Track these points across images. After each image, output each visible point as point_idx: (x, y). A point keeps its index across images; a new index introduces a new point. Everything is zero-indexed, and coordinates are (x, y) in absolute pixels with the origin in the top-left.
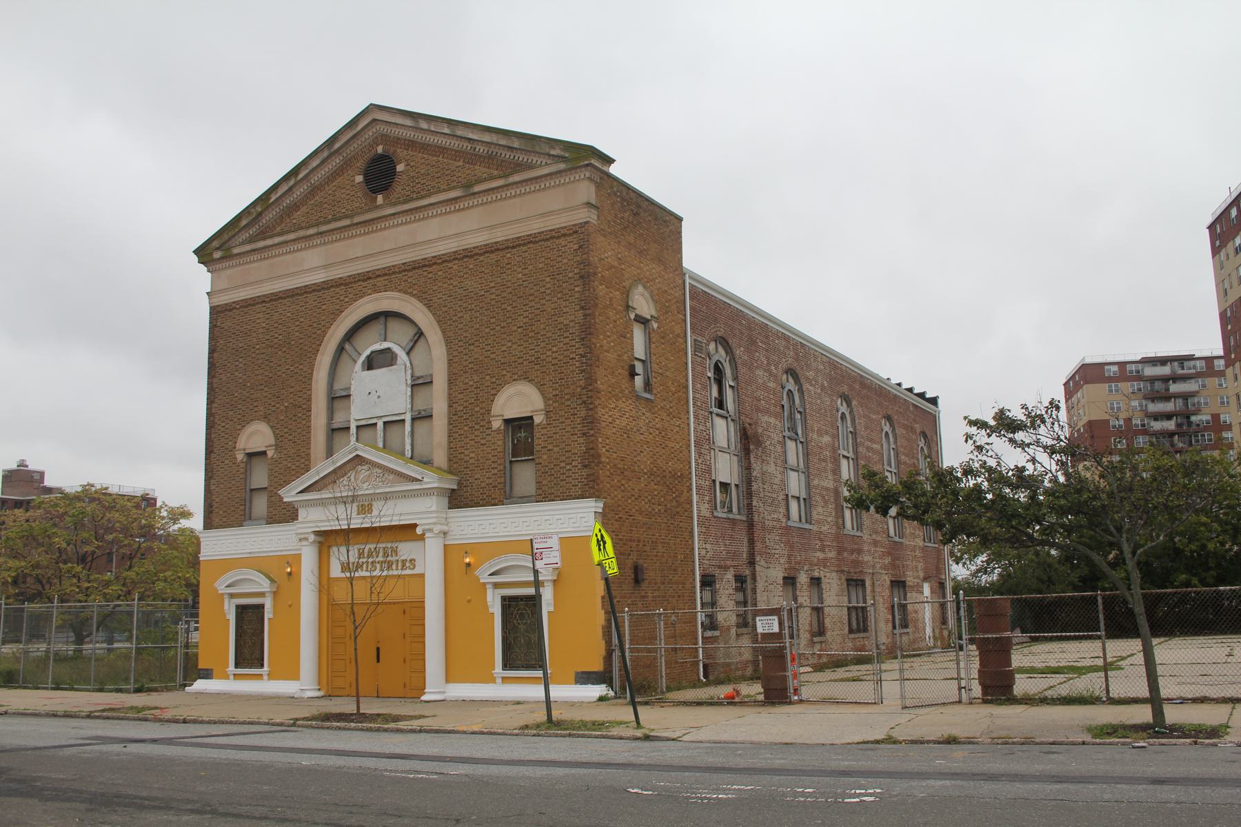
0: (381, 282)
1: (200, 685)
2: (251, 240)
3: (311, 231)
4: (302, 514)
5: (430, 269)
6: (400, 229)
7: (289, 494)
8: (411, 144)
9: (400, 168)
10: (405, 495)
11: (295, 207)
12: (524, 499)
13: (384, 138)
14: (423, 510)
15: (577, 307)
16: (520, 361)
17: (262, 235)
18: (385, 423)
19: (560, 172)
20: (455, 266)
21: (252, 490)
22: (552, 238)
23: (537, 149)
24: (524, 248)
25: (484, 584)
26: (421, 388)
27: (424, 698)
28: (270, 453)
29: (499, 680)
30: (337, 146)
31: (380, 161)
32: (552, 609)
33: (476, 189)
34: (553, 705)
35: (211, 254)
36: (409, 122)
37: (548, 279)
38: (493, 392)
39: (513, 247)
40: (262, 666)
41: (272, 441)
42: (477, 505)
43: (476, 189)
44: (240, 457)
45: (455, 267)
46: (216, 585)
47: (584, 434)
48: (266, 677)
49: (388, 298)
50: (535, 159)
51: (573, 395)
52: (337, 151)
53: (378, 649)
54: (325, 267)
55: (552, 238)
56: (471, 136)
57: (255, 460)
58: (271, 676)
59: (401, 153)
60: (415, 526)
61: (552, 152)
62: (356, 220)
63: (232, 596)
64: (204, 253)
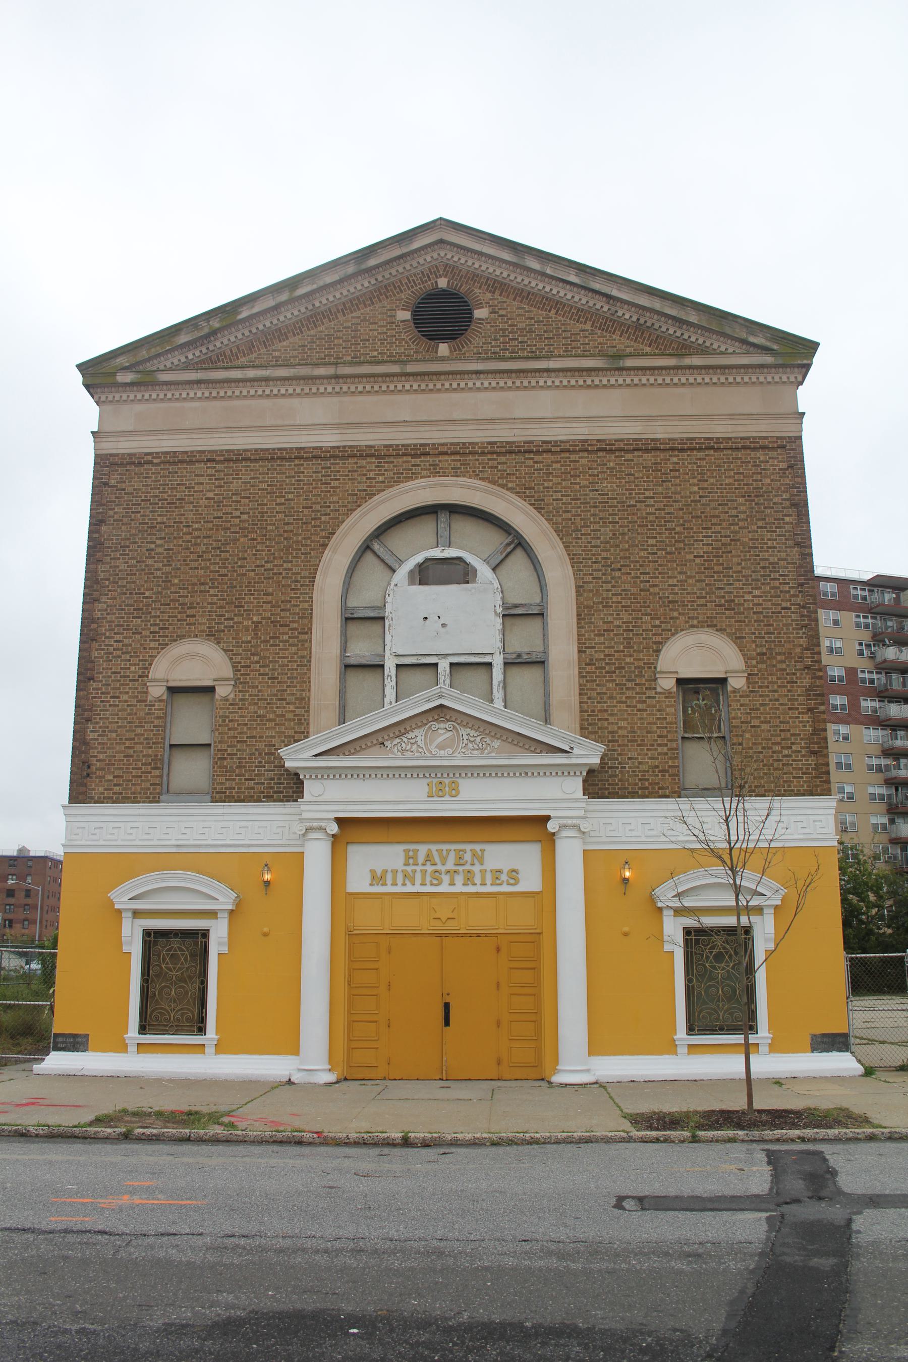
0: (446, 462)
1: (57, 1062)
2: (188, 366)
3: (322, 371)
4: (310, 788)
5: (538, 458)
6: (482, 395)
7: (295, 757)
8: (497, 286)
9: (480, 313)
10: (525, 771)
11: (280, 334)
12: (189, 795)
13: (449, 269)
14: (555, 795)
15: (790, 543)
16: (703, 601)
17: (210, 363)
18: (452, 664)
19: (762, 366)
20: (584, 460)
21: (171, 746)
22: (745, 448)
23: (728, 331)
24: (701, 455)
25: (119, 912)
26: (519, 622)
27: (557, 1079)
28: (222, 691)
29: (133, 1048)
30: (372, 262)
31: (442, 297)
32: (225, 949)
33: (629, 363)
34: (753, 1083)
35: (114, 374)
36: (506, 256)
37: (741, 500)
38: (659, 639)
39: (682, 450)
40: (202, 1030)
41: (228, 672)
42: (633, 795)
43: (629, 363)
44: (157, 691)
45: (584, 461)
46: (112, 895)
47: (810, 710)
48: (210, 1050)
49: (462, 486)
50: (716, 343)
51: (789, 655)
52: (369, 270)
53: (447, 1006)
54: (340, 426)
55: (745, 448)
56: (615, 293)
57: (182, 701)
58: (220, 1048)
59: (478, 292)
60: (547, 818)
61: (752, 339)
62: (410, 368)
63: (136, 914)
64: (98, 375)
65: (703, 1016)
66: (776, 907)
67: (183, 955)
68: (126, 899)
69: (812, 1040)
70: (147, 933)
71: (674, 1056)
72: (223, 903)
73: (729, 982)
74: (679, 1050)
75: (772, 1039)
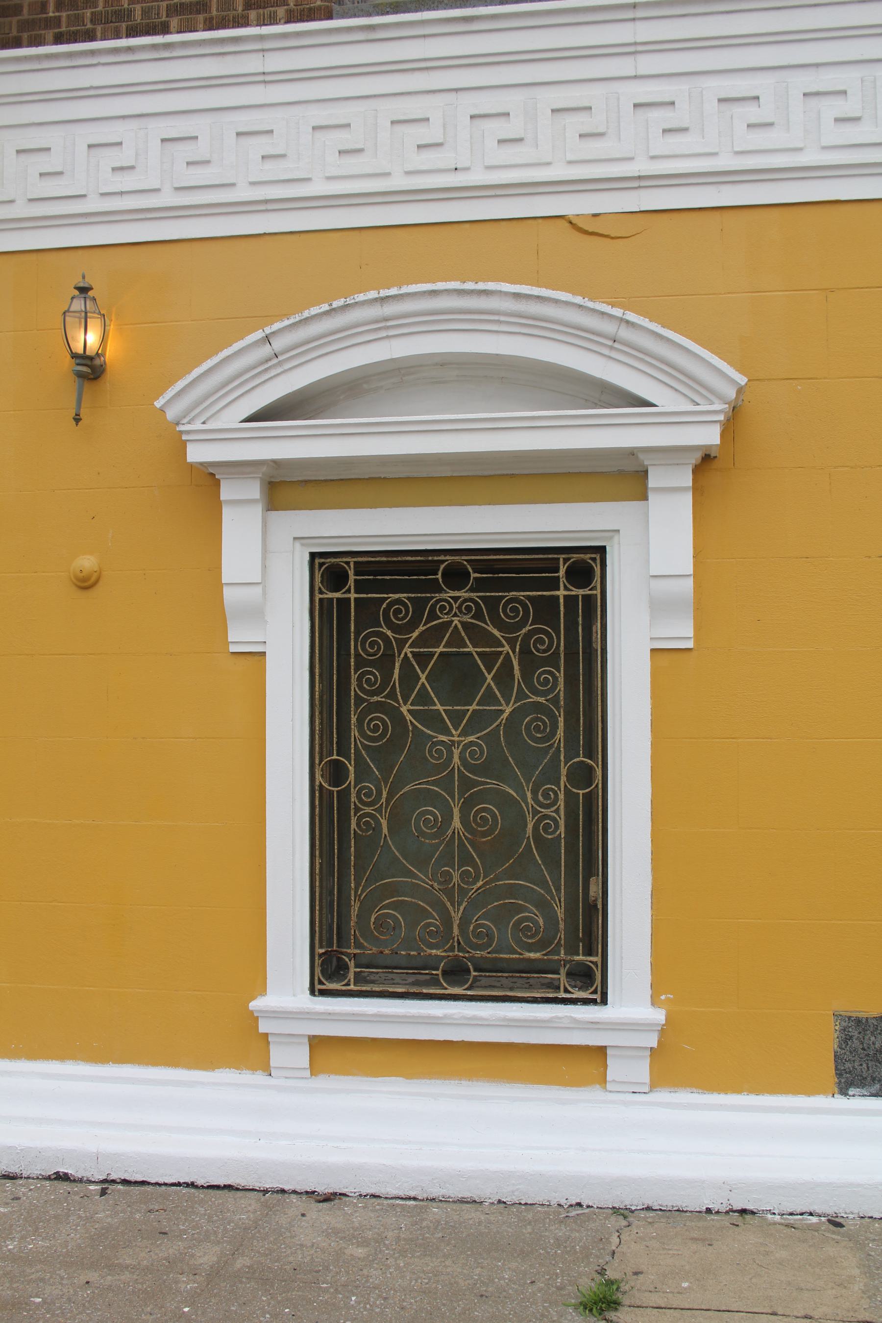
25: (208, 478)
29: (291, 1056)
32: (681, 631)
40: (588, 981)
58: (675, 1063)
63: (285, 487)
65: (381, 924)
66: (706, 462)
67: (489, 659)
68: (233, 416)
69: (845, 1039)
70: (329, 570)
71: (259, 1078)
72: (673, 420)
73: (492, 784)
74: (277, 1055)
75: (663, 1032)
